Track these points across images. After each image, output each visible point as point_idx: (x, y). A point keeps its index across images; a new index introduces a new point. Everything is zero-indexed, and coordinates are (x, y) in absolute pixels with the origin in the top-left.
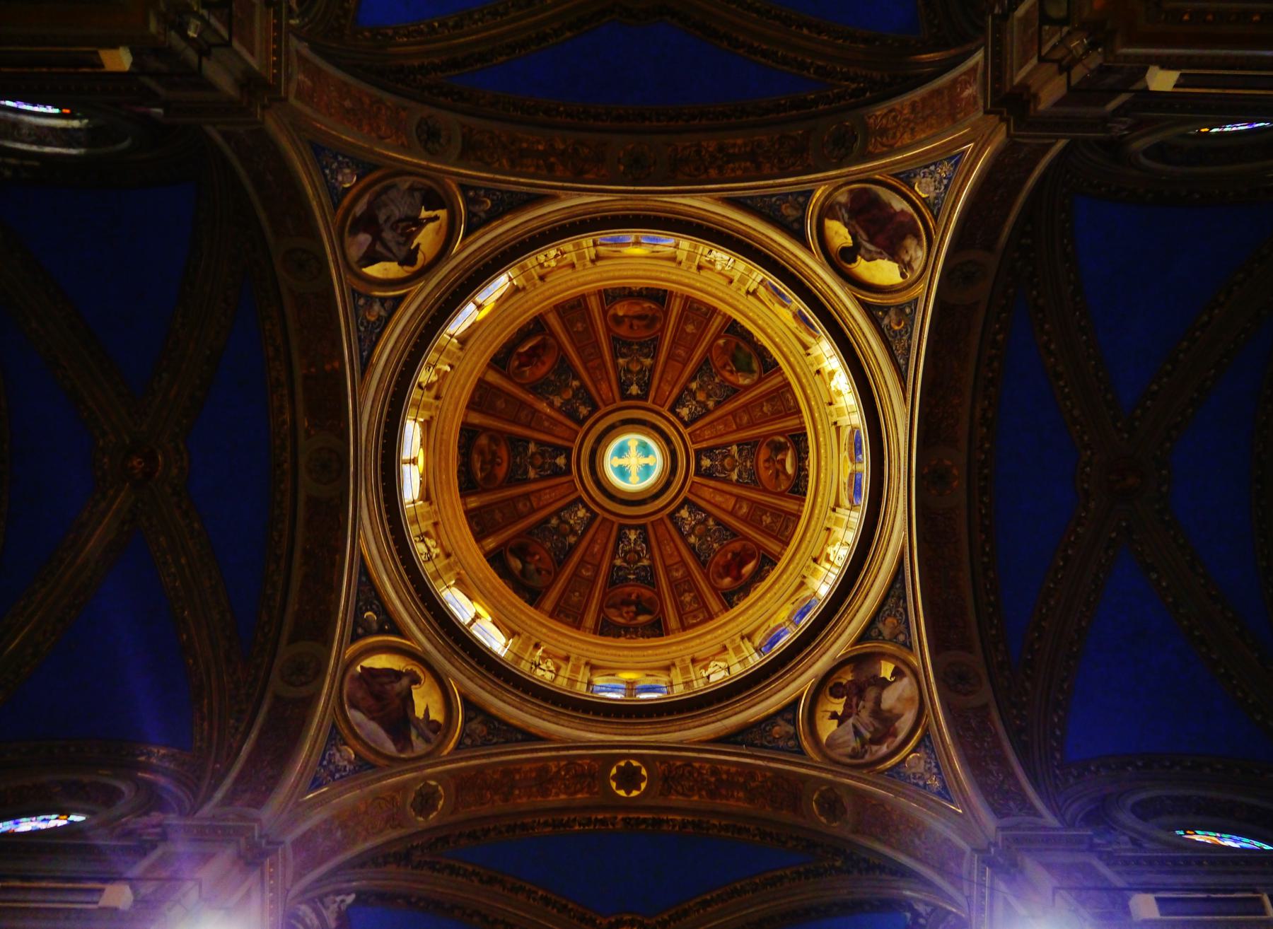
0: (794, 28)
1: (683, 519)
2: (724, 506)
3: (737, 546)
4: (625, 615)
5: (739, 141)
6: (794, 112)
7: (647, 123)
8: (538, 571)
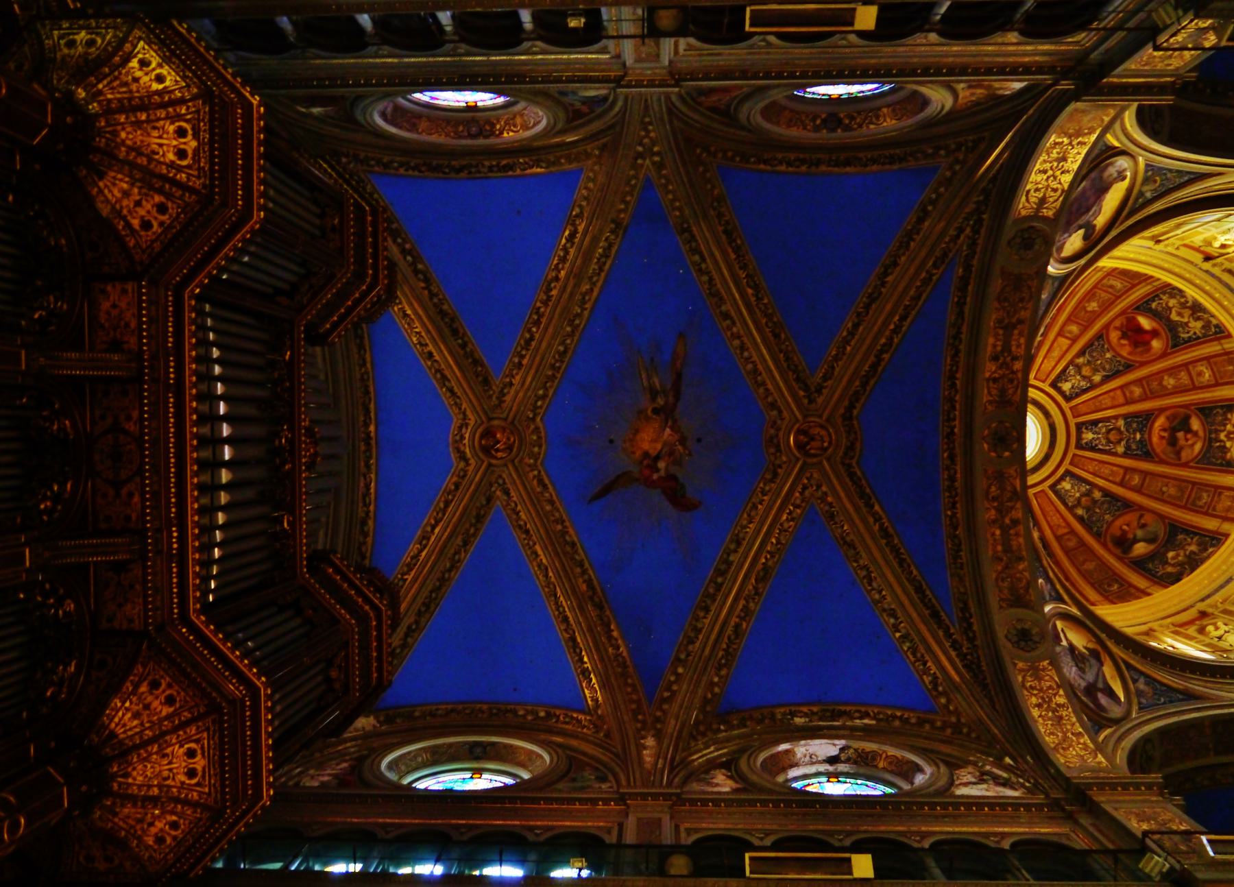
0: (883, 290)
1: (1072, 387)
2: (1064, 348)
3: (1114, 335)
4: (1190, 442)
5: (991, 340)
6: (970, 288)
7: (956, 430)
8: (1143, 526)
